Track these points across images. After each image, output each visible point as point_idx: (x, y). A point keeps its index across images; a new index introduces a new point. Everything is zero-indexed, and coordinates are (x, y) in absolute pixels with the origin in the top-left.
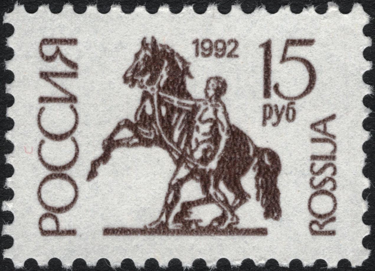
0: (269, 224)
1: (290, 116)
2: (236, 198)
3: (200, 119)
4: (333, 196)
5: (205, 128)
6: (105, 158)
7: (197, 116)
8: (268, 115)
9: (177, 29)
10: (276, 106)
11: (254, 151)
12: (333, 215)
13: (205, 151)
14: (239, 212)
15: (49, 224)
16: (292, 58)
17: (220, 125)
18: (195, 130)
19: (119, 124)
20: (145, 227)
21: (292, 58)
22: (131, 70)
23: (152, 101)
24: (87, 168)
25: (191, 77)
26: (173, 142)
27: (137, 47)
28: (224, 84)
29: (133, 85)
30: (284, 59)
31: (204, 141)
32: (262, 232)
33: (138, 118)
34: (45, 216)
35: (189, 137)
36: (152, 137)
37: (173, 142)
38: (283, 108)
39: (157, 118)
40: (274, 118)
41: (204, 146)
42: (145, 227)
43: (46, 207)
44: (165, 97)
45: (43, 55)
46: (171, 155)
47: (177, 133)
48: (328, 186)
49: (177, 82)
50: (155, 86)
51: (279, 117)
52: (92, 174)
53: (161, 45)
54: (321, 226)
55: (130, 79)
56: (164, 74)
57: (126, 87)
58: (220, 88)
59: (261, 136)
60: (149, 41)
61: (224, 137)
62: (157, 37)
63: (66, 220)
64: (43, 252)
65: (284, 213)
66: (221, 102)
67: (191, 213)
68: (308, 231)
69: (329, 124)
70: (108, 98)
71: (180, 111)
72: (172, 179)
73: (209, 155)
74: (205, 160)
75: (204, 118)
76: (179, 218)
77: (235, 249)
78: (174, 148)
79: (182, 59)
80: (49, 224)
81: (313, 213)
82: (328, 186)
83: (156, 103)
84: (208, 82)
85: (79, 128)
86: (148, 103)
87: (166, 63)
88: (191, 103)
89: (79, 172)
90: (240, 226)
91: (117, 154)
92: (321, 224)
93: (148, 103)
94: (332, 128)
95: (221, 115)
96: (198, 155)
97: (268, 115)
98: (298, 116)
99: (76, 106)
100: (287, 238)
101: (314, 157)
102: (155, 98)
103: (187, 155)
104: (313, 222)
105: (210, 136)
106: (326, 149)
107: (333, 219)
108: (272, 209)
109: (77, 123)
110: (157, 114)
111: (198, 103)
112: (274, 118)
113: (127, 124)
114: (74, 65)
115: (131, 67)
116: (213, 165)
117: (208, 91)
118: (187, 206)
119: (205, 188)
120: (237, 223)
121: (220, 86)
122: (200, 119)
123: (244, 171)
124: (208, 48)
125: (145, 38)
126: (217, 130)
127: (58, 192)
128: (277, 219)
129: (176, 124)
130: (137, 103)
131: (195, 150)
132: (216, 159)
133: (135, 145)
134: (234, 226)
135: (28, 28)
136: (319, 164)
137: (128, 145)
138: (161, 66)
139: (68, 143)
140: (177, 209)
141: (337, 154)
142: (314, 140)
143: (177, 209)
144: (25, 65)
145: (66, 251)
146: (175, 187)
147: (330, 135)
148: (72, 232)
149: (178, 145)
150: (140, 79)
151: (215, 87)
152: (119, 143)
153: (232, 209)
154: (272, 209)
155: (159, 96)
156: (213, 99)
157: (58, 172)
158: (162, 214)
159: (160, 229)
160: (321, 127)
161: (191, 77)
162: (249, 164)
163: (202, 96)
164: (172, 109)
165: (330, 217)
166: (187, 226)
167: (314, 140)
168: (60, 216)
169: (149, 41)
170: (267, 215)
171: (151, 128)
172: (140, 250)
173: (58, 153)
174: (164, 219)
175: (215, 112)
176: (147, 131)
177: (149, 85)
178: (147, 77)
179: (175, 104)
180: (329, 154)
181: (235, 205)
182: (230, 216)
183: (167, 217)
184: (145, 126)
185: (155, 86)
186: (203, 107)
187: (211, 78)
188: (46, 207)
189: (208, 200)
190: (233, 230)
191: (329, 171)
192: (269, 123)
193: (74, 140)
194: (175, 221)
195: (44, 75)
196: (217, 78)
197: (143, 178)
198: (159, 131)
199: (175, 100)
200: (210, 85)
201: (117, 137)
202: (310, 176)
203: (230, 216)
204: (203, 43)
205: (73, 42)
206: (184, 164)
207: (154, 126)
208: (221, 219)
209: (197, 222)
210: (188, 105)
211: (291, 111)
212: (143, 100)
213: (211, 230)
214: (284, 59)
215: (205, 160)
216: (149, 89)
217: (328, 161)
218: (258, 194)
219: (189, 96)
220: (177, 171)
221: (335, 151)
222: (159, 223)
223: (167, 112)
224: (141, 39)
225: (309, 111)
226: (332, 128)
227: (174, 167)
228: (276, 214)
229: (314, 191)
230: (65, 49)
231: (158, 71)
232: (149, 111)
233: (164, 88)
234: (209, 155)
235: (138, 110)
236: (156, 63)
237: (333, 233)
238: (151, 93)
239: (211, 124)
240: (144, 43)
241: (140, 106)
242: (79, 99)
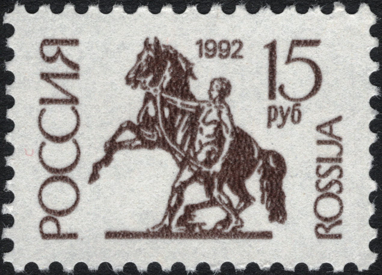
0: (274, 227)
1: (296, 118)
2: (240, 201)
3: (204, 121)
4: (339, 199)
5: (209, 130)
6: (107, 160)
8: (273, 117)
9: (180, 30)
10: (281, 107)
11: (259, 154)
12: (339, 219)
13: (209, 153)
14: (243, 215)
15: (50, 228)
16: (298, 59)
17: (224, 127)
18: (199, 132)
19: (121, 126)
20: (148, 230)
21: (298, 59)
22: (134, 71)
23: (155, 103)
24: (89, 170)
25: (195, 78)
26: (176, 144)
27: (140, 48)
28: (229, 85)
29: (135, 86)
30: (289, 60)
31: (208, 143)
32: (267, 235)
33: (141, 120)
34: (46, 219)
35: (193, 139)
36: (155, 139)
37: (176, 144)
38: (288, 110)
40: (279, 120)
41: (208, 148)
42: (148, 230)
44: (168, 99)
45: (43, 56)
46: (174, 157)
47: (180, 135)
48: (334, 189)
49: (181, 83)
50: (158, 88)
51: (284, 118)
52: (94, 177)
53: (164, 46)
54: (327, 230)
55: (132, 80)
56: (167, 75)
57: (128, 88)
58: (224, 89)
59: (266, 138)
60: (152, 41)
61: (229, 139)
63: (67, 224)
64: (44, 255)
65: (289, 216)
66: (226, 104)
67: (194, 216)
68: (314, 235)
69: (335, 126)
70: (110, 99)
71: (184, 113)
72: (175, 182)
73: (212, 157)
74: (208, 162)
75: (208, 120)
76: (182, 221)
78: (177, 150)
79: (185, 60)
80: (50, 228)
81: (319, 217)
82: (334, 189)
83: (158, 105)
84: (212, 83)
85: (81, 130)
86: (150, 104)
87: (169, 64)
88: (195, 104)
89: (81, 175)
90: (245, 229)
91: (119, 156)
92: (327, 228)
93: (150, 104)
94: (338, 129)
95: (225, 117)
96: (202, 157)
97: (273, 117)
98: (303, 117)
99: (77, 107)
100: (293, 242)
101: (320, 160)
102: (158, 99)
103: (190, 157)
104: (318, 226)
105: (214, 139)
106: (332, 151)
107: (339, 223)
108: (278, 212)
109: (78, 124)
110: (160, 115)
111: (202, 105)
112: (279, 120)
113: (130, 126)
114: (75, 66)
115: (133, 68)
116: (217, 167)
117: (212, 92)
118: (191, 209)
119: (209, 191)
120: (242, 226)
121: (224, 87)
122: (204, 121)
123: (249, 173)
124: (211, 49)
125: (147, 39)
126: (221, 132)
127: (59, 195)
128: (282, 222)
129: (179, 126)
130: (140, 105)
131: (199, 152)
132: (220, 162)
133: (137, 147)
134: (238, 229)
135: (29, 28)
136: (325, 167)
137: (130, 147)
138: (164, 67)
139: (69, 144)
140: (181, 212)
141: (344, 157)
142: (320, 142)
143: (181, 212)
144: (25, 66)
145: (67, 255)
146: (178, 190)
147: (336, 137)
148: (73, 236)
149: (181, 147)
150: (142, 80)
151: (219, 89)
152: (121, 146)
153: (237, 213)
154: (278, 212)
155: (162, 98)
156: (217, 100)
157: (59, 175)
158: (165, 217)
159: (163, 232)
160: (327, 129)
161: (195, 78)
162: (254, 167)
163: (206, 97)
164: (175, 111)
165: (336, 220)
166: (190, 230)
167: (320, 142)
168: (61, 219)
169: (152, 41)
170: (272, 218)
171: (154, 130)
173: (60, 155)
174: (167, 222)
175: (219, 114)
176: (150, 133)
177: (152, 86)
178: (149, 79)
179: (179, 106)
180: (335, 156)
181: (239, 208)
182: (234, 219)
183: (170, 220)
184: (148, 128)
185: (158, 88)
186: (207, 109)
187: (215, 79)
189: (212, 202)
190: (237, 234)
191: (335, 174)
192: (274, 124)
193: (76, 143)
194: (178, 224)
195: (45, 76)
196: (221, 80)
197: (146, 180)
198: (162, 133)
199: (179, 102)
200: (214, 87)
201: (119, 139)
202: (316, 178)
203: (234, 219)
204: (206, 44)
205: (75, 42)
206: (188, 167)
207: (157, 128)
208: (225, 222)
209: (200, 225)
210: (191, 107)
211: (296, 113)
212: (146, 101)
213: (215, 233)
214: (289, 60)
215: (208, 162)
216: (151, 90)
217: (334, 164)
218: (263, 197)
219: (192, 97)
220: (180, 173)
221: (341, 153)
222: (162, 226)
223: (170, 114)
224: (144, 39)
225: (314, 112)
226: (338, 129)
227: (177, 170)
228: (281, 218)
229: (320, 194)
230: (66, 50)
231: (161, 72)
232: (152, 112)
234: (212, 157)
235: (140, 112)
237: (339, 236)
238: (154, 94)
239: (215, 126)
240: (146, 44)
241: (143, 108)
242: (80, 101)
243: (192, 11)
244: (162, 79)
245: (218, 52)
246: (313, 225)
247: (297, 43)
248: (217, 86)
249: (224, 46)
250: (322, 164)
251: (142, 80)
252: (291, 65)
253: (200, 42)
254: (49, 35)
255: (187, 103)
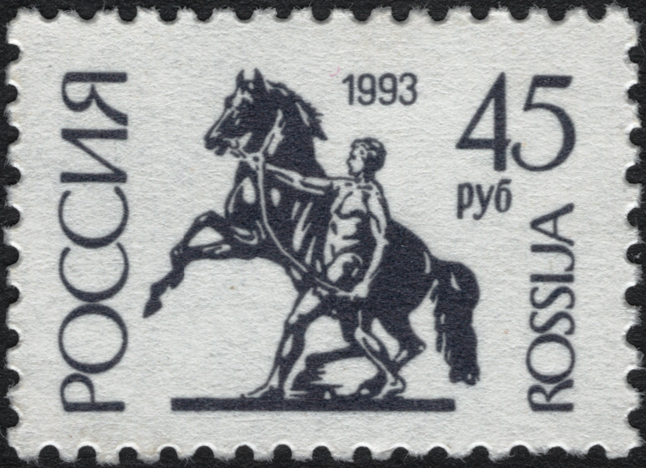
0: (458, 391)
2: (401, 350)
4: (567, 344)
5: (348, 227)
6: (174, 279)
7: (334, 207)
8: (466, 201)
9: (307, 55)
10: (479, 187)
11: (432, 266)
13: (347, 267)
14: (405, 372)
15: (78, 393)
17: (373, 222)
22: (218, 126)
23: (255, 181)
24: (145, 295)
25: (323, 137)
27: (229, 87)
30: (529, 106)
31: (345, 250)
32: (447, 405)
38: (492, 188)
39: (264, 213)
40: (476, 207)
41: (347, 258)
43: (78, 294)
44: (276, 173)
45: (66, 99)
46: (288, 272)
48: (560, 328)
50: (259, 155)
51: (484, 203)
54: (549, 397)
55: (217, 142)
56: (276, 137)
57: (211, 154)
58: (374, 157)
60: (249, 75)
61: (382, 243)
62: (263, 72)
63: (106, 386)
64: (68, 436)
66: (376, 183)
67: (323, 373)
68: (526, 404)
70: (183, 176)
72: (291, 315)
74: (348, 281)
75: (346, 210)
76: (299, 383)
77: (382, 434)
79: (308, 108)
80: (78, 393)
82: (560, 328)
83: (261, 185)
84: (354, 146)
85: (130, 227)
87: (280, 116)
91: (196, 270)
92: (550, 392)
94: (565, 226)
95: (375, 206)
96: (335, 273)
97: (466, 201)
98: (515, 200)
99: (123, 187)
100: (495, 415)
101: (536, 278)
102: (260, 174)
104: (533, 390)
106: (556, 264)
107: (569, 384)
108: (464, 366)
109: (125, 217)
111: (337, 184)
112: (476, 207)
113: (210, 220)
114: (121, 118)
115: (218, 122)
116: (361, 290)
118: (318, 361)
119: (348, 333)
120: (402, 390)
122: (338, 212)
123: (414, 304)
124: (366, 88)
127: (93, 339)
128: (472, 383)
129: (296, 221)
130: (229, 186)
131: (330, 264)
133: (224, 256)
136: (545, 290)
137: (212, 256)
139: (110, 253)
140: (299, 366)
141: (576, 273)
142: (537, 248)
143: (299, 366)
145: (107, 438)
146: (296, 330)
147: (565, 240)
148: (118, 407)
149: (300, 256)
150: (233, 142)
151: (365, 156)
152: (199, 254)
153: (395, 367)
154: (464, 366)
156: (361, 176)
157: (92, 304)
158: (272, 375)
159: (269, 401)
160: (548, 226)
161: (323, 137)
163: (344, 171)
164: (289, 194)
165: (563, 381)
166: (316, 397)
167: (537, 248)
168: (96, 379)
169: (249, 75)
170: (455, 377)
172: (224, 435)
173: (94, 271)
174: (275, 382)
175: (366, 199)
178: (244, 140)
181: (399, 359)
182: (390, 377)
184: (244, 225)
185: (259, 155)
186: (344, 191)
188: (78, 294)
189: (353, 351)
190: (397, 403)
192: (469, 213)
193: (120, 247)
194: (295, 387)
195: (72, 136)
196: (368, 141)
197: (242, 313)
198: (267, 233)
199: (296, 179)
201: (195, 242)
202: (530, 309)
205: (120, 78)
207: (258, 223)
208: (375, 384)
209: (331, 388)
211: (504, 194)
214: (529, 106)
215: (348, 281)
216: (249, 159)
217: (561, 285)
218: (439, 341)
220: (297, 302)
221: (571, 268)
224: (236, 74)
225: (533, 194)
226: (565, 226)
227: (295, 294)
228: (469, 377)
229: (536, 335)
230: (105, 90)
231: (266, 129)
232: (249, 195)
233: (277, 154)
234: (354, 273)
235: (230, 196)
236: (264, 115)
237: (568, 407)
238: (253, 165)
240: (241, 83)
241: (234, 189)
243: (302, 17)
244: (267, 139)
245: (379, 94)
246: (540, 365)
247: (540, 81)
248: (362, 153)
249: (388, 84)
250: (540, 285)
251: (233, 142)
252: (531, 114)
253: (349, 79)
254: (80, 66)
255: (310, 180)
